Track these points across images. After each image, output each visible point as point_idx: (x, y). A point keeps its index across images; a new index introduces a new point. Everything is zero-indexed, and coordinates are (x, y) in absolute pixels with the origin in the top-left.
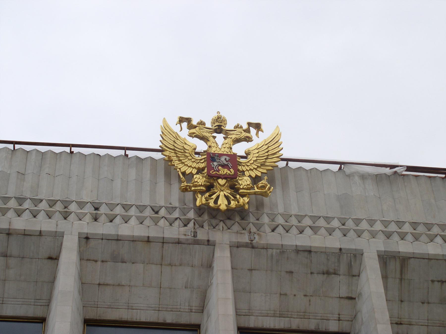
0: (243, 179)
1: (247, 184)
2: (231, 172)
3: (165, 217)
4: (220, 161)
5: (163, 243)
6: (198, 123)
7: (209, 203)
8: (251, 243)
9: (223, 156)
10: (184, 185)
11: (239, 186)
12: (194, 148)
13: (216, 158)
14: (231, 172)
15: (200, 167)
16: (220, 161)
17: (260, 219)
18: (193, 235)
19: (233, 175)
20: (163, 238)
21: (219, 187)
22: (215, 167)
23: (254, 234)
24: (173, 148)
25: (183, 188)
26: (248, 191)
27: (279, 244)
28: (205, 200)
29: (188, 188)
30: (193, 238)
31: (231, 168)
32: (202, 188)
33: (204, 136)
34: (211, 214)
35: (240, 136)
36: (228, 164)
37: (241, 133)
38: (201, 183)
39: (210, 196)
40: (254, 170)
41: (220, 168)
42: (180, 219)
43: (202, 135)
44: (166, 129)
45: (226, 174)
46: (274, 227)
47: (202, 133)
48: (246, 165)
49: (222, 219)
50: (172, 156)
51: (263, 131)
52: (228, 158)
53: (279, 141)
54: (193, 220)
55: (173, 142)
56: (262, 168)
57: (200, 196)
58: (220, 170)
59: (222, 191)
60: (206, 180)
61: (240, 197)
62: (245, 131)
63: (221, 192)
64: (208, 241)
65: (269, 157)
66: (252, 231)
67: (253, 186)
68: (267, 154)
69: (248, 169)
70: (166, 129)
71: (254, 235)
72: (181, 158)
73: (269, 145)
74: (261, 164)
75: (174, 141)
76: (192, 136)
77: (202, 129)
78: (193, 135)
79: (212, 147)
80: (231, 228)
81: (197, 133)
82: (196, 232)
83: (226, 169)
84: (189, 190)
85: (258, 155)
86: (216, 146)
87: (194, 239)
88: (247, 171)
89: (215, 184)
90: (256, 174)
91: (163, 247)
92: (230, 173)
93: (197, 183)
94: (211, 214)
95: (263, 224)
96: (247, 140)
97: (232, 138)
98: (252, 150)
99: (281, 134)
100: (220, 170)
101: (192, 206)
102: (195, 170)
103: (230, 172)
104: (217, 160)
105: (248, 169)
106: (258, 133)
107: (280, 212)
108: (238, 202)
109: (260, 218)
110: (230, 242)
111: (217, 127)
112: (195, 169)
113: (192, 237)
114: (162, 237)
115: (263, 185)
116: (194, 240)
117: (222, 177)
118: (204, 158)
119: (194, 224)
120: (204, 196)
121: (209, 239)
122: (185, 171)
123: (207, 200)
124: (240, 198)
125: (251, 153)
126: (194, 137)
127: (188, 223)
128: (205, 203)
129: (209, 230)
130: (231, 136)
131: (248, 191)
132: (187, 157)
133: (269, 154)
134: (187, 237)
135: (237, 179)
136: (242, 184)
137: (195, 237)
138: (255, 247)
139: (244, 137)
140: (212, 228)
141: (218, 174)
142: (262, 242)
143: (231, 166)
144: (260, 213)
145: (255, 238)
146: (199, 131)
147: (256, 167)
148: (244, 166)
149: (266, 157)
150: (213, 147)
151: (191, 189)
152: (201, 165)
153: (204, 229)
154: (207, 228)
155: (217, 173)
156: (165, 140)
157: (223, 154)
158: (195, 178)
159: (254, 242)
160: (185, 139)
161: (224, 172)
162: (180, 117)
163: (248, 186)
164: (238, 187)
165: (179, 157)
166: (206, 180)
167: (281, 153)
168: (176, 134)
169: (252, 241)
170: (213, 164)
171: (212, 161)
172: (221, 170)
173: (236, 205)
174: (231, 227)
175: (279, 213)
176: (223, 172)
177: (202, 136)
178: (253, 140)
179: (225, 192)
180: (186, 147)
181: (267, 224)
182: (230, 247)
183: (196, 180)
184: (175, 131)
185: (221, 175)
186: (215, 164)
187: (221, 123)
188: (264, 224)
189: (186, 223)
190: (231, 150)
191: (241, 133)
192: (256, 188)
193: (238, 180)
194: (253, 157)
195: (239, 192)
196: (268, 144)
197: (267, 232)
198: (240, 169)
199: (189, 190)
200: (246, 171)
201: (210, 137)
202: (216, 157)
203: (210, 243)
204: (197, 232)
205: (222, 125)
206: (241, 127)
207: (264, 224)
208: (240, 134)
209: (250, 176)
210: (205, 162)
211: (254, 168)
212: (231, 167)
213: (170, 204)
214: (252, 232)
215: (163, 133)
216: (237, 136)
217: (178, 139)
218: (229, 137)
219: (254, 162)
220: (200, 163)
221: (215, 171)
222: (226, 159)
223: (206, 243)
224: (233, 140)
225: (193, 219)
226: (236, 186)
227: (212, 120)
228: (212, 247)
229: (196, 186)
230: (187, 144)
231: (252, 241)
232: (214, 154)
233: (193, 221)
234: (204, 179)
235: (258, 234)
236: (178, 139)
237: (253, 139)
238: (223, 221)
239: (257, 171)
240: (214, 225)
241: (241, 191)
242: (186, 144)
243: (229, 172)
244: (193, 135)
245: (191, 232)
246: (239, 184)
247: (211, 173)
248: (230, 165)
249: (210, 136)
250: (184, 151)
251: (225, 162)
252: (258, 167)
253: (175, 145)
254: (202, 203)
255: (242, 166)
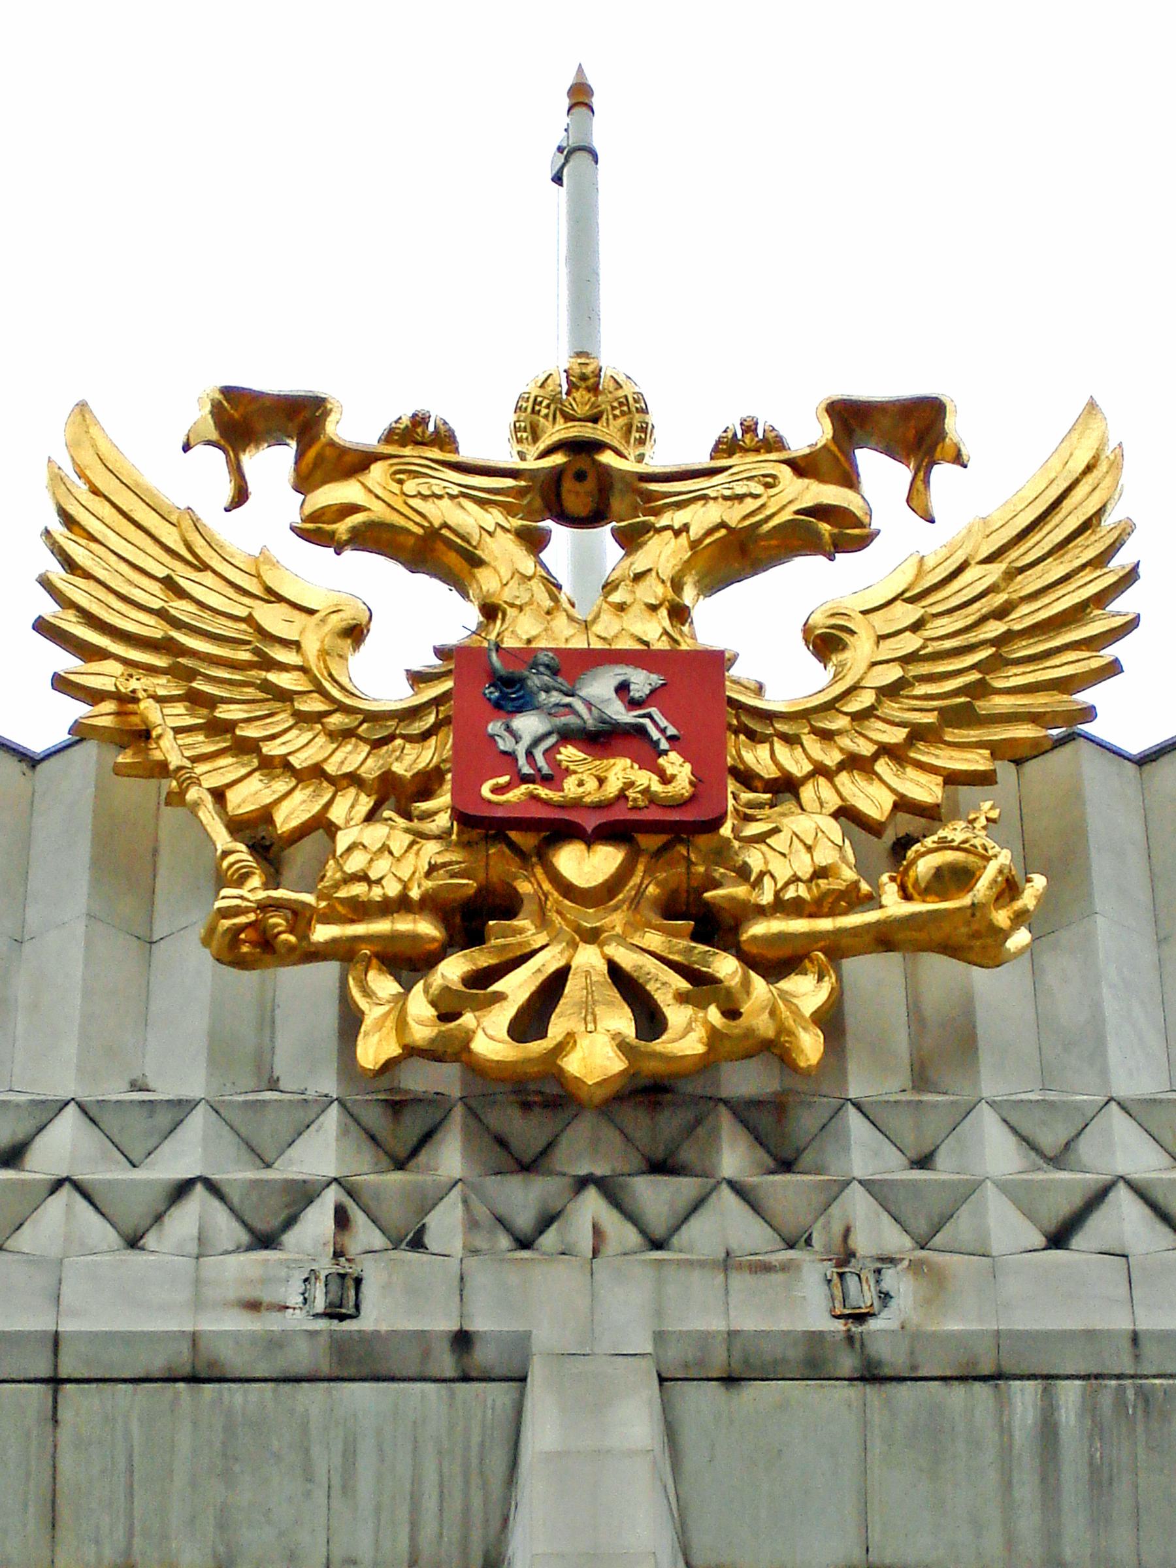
0: (776, 831)
1: (811, 870)
2: (666, 780)
3: (78, 1187)
4: (568, 705)
5: (55, 1382)
6: (391, 436)
7: (469, 1036)
8: (850, 1338)
9: (600, 669)
10: (238, 902)
11: (741, 891)
12: (344, 624)
13: (534, 681)
14: (666, 780)
15: (394, 773)
16: (568, 700)
17: (941, 1159)
18: (320, 1305)
19: (682, 804)
20: (50, 1345)
21: (559, 912)
22: (529, 754)
23: (879, 1265)
24: (159, 635)
25: (226, 923)
26: (825, 924)
27: (1094, 1330)
28: (431, 1012)
29: (276, 925)
30: (322, 1324)
31: (665, 752)
32: (404, 924)
33: (436, 524)
34: (501, 1142)
35: (763, 506)
36: (646, 721)
37: (768, 486)
38: (399, 887)
39: (481, 979)
40: (883, 767)
41: (569, 753)
42: (213, 1187)
43: (418, 519)
44: (96, 491)
45: (622, 796)
46: (1061, 1207)
47: (416, 503)
48: (815, 731)
49: (599, 1171)
50: (141, 694)
51: (958, 459)
52: (642, 681)
53: (1109, 520)
54: (334, 1186)
55: (155, 587)
56: (947, 738)
57: (385, 985)
58: (567, 769)
59: (593, 936)
60: (447, 857)
61: (752, 974)
62: (802, 467)
63: (581, 945)
64: (462, 1340)
65: (1014, 651)
66: (862, 1243)
67: (865, 887)
68: (994, 629)
69: (832, 758)
70: (96, 491)
71: (878, 1271)
72: (226, 712)
73: (1019, 556)
74: (941, 710)
75: (169, 583)
76: (332, 534)
77: (416, 475)
78: (342, 528)
79: (509, 610)
80: (675, 1240)
81: (379, 511)
82: (350, 1283)
83: (628, 762)
84: (284, 936)
85: (919, 642)
86: (548, 603)
87: (331, 1333)
88: (822, 780)
89: (524, 887)
90: (901, 789)
91: (55, 1421)
92: (657, 787)
93: (358, 889)
94: (501, 1142)
95: (969, 1190)
96: (818, 534)
97: (686, 528)
98: (864, 613)
99: (1116, 465)
100: (572, 768)
101: (329, 1084)
102: (356, 800)
103: (655, 778)
104: (543, 695)
105: (832, 758)
106: (926, 482)
107: (1123, 1088)
108: (732, 1014)
109: (938, 1147)
110: (660, 1337)
111: (558, 459)
112: (352, 791)
113: (316, 1316)
114: (45, 1332)
115: (949, 856)
116: (340, 1347)
117: (590, 823)
118: (437, 701)
119: (342, 1219)
120: (420, 986)
121: (466, 1328)
122: (265, 815)
123: (446, 1017)
124: (746, 984)
125: (852, 632)
126: (347, 543)
127: (290, 1222)
128: (432, 1041)
129: (472, 1262)
130: (678, 518)
131: (825, 924)
132: (284, 696)
133: (1018, 627)
134: (273, 1323)
135: (726, 830)
136: (771, 867)
137: (342, 1318)
138: (887, 1371)
139: (798, 512)
140: (505, 1242)
141: (547, 803)
142: (954, 1326)
143: (671, 739)
144: (935, 1105)
145: (885, 1297)
146: (395, 487)
147: (896, 736)
148: (791, 740)
149: (991, 651)
150: (521, 608)
151: (304, 936)
152: (408, 760)
153: (425, 1257)
154: (457, 1246)
155: (543, 792)
156: (88, 576)
157: (610, 650)
158: (350, 849)
159: (873, 1325)
160: (264, 558)
161: (601, 781)
162: (227, 391)
163: (821, 882)
164: (732, 899)
165: (212, 702)
166: (440, 860)
167: (1123, 610)
168: (187, 524)
169: (860, 1318)
170: (508, 729)
171: (498, 705)
172: (575, 772)
173: (714, 1036)
174: (677, 1228)
175: (1111, 1099)
176: (591, 784)
177: (420, 531)
178: (878, 532)
179: (613, 950)
180: (272, 618)
181: (1004, 1187)
182: (662, 1380)
183: (354, 864)
184: (176, 496)
185: (576, 804)
186: (529, 724)
187: (595, 419)
188: (980, 1183)
189: (276, 1222)
190: (686, 629)
191: (768, 486)
192: (890, 895)
193: (728, 840)
194: (874, 664)
195: (744, 937)
196: (1013, 554)
197: (996, 1249)
198: (758, 769)
199: (284, 936)
200: (811, 775)
201: (490, 534)
202: (535, 677)
203: (484, 1356)
204: (358, 1281)
205: (607, 439)
206: (773, 443)
207: (980, 1183)
208: (758, 489)
209: (846, 814)
210: (444, 730)
211: (885, 750)
212: (664, 745)
213: (135, 1086)
214: (860, 1252)
215: (68, 520)
216: (734, 515)
217: (204, 567)
218: (664, 520)
219: (878, 700)
220: (399, 742)
221: (526, 779)
222: (623, 688)
223: (446, 1364)
224: (700, 541)
225: (328, 1185)
226: (720, 892)
227: (518, 409)
228: (498, 1394)
229: (360, 910)
230: (280, 599)
231: (860, 1318)
232: (527, 656)
233: (332, 1196)
234: (431, 850)
235: (916, 1267)
236: (204, 567)
237: (874, 526)
238: (605, 1186)
239: (910, 771)
240: (524, 1221)
241: (759, 928)
242: (273, 596)
243: (645, 778)
244: (342, 528)
245: (306, 1280)
246: (743, 872)
247: (489, 802)
248: (663, 731)
249: (491, 529)
250: (257, 652)
251: (620, 713)
252: (918, 734)
253: (181, 609)
254: (407, 1040)
255: (779, 746)
